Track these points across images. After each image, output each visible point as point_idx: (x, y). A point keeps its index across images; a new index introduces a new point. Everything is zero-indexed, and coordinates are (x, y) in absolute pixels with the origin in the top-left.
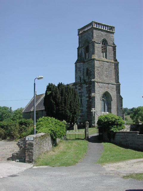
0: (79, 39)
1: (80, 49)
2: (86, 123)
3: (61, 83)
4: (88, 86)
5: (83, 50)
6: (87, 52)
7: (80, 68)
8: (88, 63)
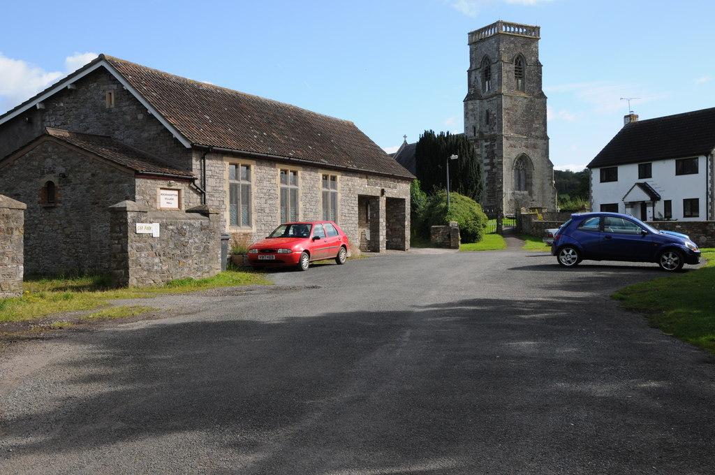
1: (473, 73)
3: (448, 133)
4: (488, 143)
5: (478, 75)
6: (486, 80)
7: (473, 110)
8: (488, 100)
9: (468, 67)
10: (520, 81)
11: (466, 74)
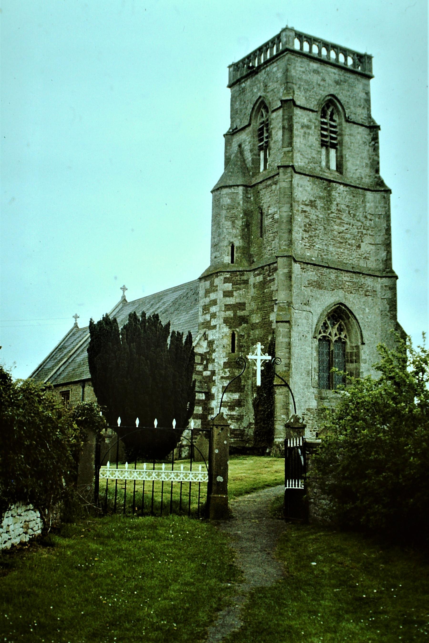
0: (233, 100)
2: (275, 384)
9: (226, 126)
10: (333, 152)
11: (223, 140)
